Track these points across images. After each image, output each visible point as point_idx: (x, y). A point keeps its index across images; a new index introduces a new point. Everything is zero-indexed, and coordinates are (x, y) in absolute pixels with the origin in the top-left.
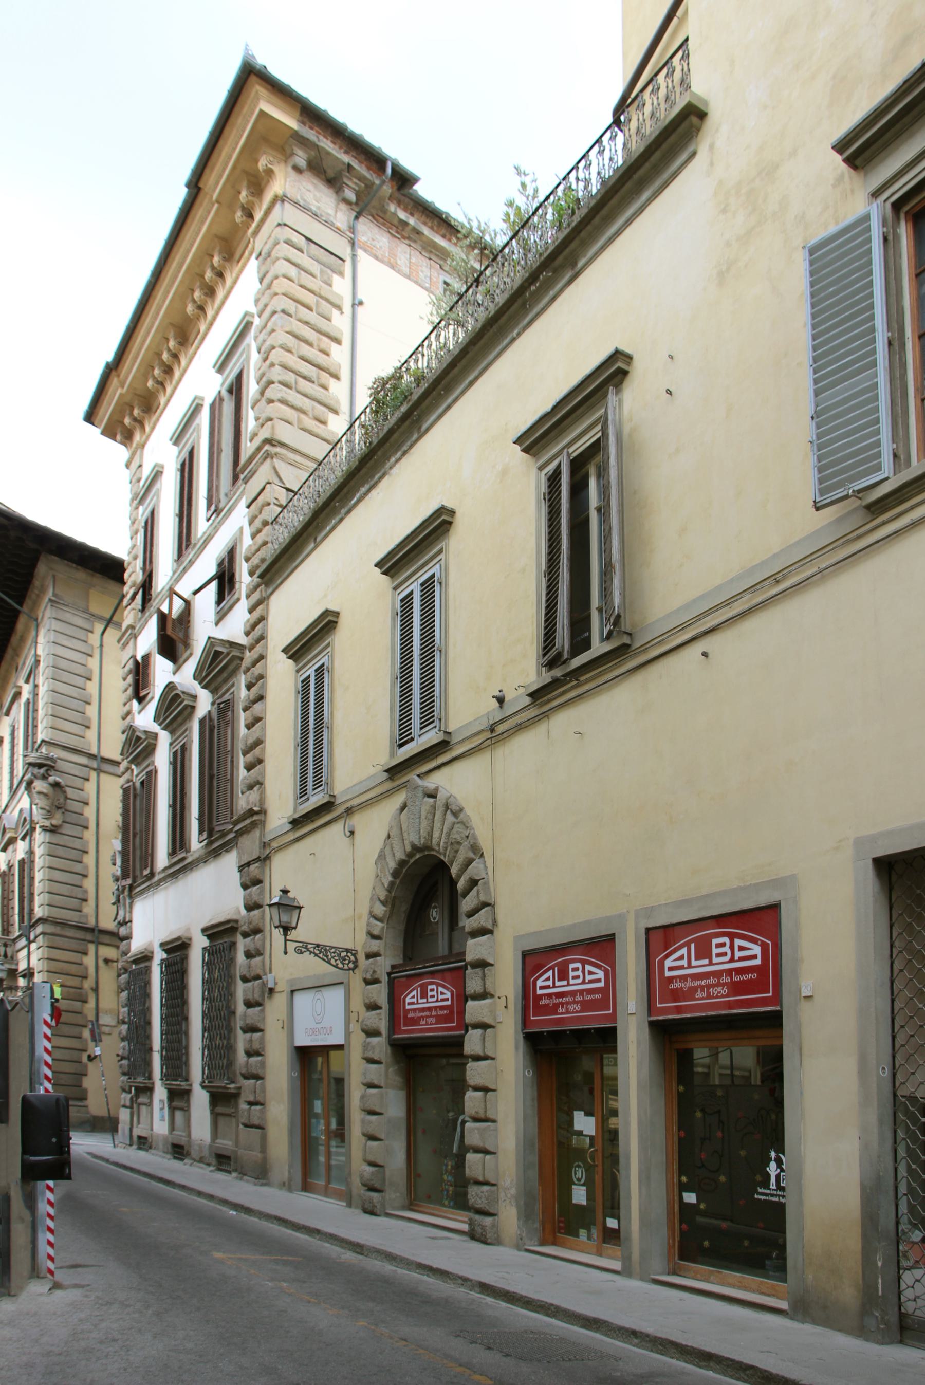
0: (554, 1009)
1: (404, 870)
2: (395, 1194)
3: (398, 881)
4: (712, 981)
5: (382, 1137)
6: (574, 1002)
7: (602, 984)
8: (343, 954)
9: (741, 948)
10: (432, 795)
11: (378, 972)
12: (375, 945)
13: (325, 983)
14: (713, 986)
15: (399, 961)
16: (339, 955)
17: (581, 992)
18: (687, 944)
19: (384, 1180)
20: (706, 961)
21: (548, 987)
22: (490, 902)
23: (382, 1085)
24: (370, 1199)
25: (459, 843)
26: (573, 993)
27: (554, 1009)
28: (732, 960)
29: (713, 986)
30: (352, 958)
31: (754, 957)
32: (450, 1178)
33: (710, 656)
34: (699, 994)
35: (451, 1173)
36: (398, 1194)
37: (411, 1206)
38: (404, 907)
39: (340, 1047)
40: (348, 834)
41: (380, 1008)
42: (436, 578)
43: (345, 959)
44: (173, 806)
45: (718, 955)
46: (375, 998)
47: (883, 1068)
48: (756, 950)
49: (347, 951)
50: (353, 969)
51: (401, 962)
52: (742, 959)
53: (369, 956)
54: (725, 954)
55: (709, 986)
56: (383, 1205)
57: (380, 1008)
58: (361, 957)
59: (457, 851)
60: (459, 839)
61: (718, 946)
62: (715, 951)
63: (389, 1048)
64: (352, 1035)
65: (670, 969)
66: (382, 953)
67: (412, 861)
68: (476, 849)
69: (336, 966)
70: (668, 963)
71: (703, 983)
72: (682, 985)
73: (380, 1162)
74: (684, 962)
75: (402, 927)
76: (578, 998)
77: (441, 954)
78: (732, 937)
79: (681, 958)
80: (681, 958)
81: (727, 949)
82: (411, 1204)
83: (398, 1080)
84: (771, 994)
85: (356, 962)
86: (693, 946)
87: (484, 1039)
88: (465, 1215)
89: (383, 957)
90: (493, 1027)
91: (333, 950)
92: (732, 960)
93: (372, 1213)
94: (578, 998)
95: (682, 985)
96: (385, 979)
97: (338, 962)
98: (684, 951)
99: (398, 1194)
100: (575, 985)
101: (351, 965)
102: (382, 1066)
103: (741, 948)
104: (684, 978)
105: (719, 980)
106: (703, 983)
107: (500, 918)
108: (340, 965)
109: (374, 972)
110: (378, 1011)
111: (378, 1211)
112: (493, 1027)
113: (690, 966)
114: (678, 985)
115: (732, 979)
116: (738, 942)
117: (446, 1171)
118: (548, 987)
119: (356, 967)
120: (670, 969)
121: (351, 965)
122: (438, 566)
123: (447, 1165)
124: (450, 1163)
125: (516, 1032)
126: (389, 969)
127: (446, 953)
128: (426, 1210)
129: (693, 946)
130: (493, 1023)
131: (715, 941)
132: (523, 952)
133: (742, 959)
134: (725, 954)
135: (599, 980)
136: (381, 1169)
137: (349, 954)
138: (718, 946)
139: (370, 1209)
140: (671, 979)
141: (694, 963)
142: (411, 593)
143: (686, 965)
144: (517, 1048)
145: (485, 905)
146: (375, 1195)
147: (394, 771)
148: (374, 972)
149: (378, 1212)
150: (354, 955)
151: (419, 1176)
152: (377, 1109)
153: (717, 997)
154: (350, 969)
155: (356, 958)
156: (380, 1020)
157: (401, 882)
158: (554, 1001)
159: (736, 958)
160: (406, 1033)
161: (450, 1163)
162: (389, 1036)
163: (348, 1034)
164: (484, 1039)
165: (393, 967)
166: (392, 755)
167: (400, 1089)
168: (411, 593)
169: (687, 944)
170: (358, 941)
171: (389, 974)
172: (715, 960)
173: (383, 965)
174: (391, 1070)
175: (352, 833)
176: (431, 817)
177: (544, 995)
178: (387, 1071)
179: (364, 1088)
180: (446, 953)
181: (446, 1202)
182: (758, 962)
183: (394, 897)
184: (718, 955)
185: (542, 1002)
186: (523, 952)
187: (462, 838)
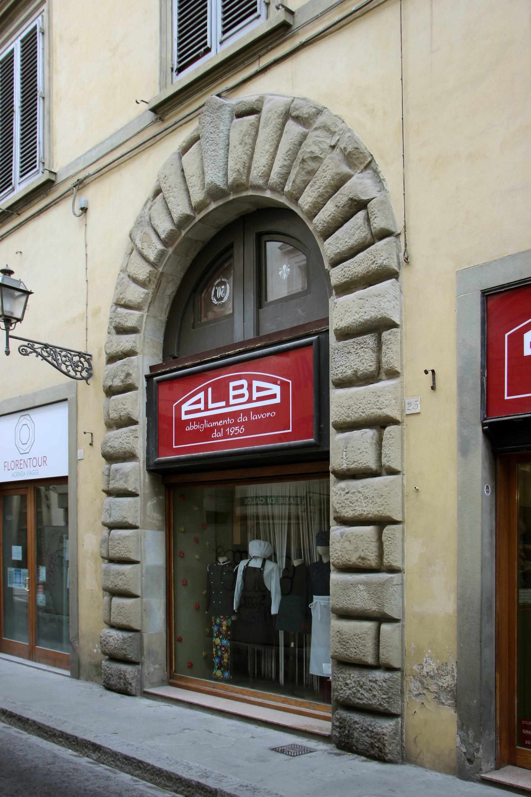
0: (207, 434)
1: (183, 233)
2: (154, 667)
3: (170, 250)
4: (229, 421)
5: (139, 593)
6: (236, 424)
7: (277, 400)
8: (76, 359)
9: (259, 389)
10: (253, 111)
11: (134, 375)
12: (126, 342)
13: (37, 404)
14: (230, 426)
15: (158, 361)
16: (71, 360)
17: (246, 412)
18: (205, 389)
19: (141, 648)
20: (223, 404)
21: (199, 411)
22: (393, 230)
23: (138, 524)
24: (117, 672)
25: (315, 158)
26: (235, 415)
27: (207, 434)
28: (250, 400)
29: (230, 426)
30: (86, 365)
31: (274, 396)
32: (225, 642)
33: (23, 253)
34: (215, 435)
35: (226, 637)
36: (157, 666)
37: (172, 679)
38: (170, 290)
39: (63, 480)
40: (78, 212)
41: (135, 423)
42: (38, 30)
43: (75, 364)
44: (6, 42)
45: (235, 397)
46: (129, 409)
47: (487, 487)
48: (276, 389)
49: (80, 355)
50: (86, 379)
51: (160, 362)
52: (259, 399)
53: (112, 359)
54: (242, 396)
55: (225, 426)
56: (141, 683)
57: (135, 423)
58: (99, 363)
59: (311, 173)
60: (317, 152)
61: (235, 388)
62: (232, 393)
63: (147, 475)
64: (81, 464)
65: (187, 413)
66: (138, 350)
67: (199, 217)
68: (358, 159)
69: (67, 374)
70: (185, 407)
71: (220, 423)
72: (198, 427)
73: (135, 625)
74: (201, 406)
75: (164, 317)
76: (241, 419)
77: (238, 337)
78: (250, 379)
79: (198, 402)
80: (198, 402)
81: (245, 391)
82: (171, 676)
83: (155, 517)
84: (174, 447)
85: (90, 369)
86: (210, 390)
87: (379, 443)
88: (324, 709)
89: (139, 356)
90: (395, 422)
91: (64, 353)
92: (250, 400)
93: (125, 692)
94: (241, 419)
95: (198, 427)
96: (142, 384)
97: (70, 368)
98: (201, 395)
99: (157, 666)
100: (237, 405)
101: (84, 374)
102: (137, 499)
103: (259, 389)
104: (200, 420)
105: (236, 420)
106: (220, 423)
107: (415, 251)
108: (72, 373)
109: (128, 375)
110: (133, 427)
111: (134, 687)
112: (395, 422)
113: (206, 409)
114: (194, 427)
115: (249, 418)
116: (256, 384)
117: (219, 633)
118: (199, 411)
119: (90, 375)
120: (187, 413)
121: (84, 374)
122: (40, 18)
123: (220, 625)
124: (225, 623)
125: (463, 423)
126: (147, 372)
127: (251, 335)
128: (190, 685)
129: (210, 390)
130: (399, 418)
131: (232, 384)
132: (483, 292)
133: (259, 399)
134: (242, 396)
135: (274, 396)
136: (137, 635)
137: (82, 360)
138: (235, 388)
139: (122, 686)
140: (187, 422)
141: (211, 406)
142: (12, 51)
143: (203, 409)
144: (464, 450)
145: (384, 234)
146: (128, 669)
147: (161, 110)
148: (128, 375)
149: (134, 692)
150: (88, 361)
151: (180, 640)
152: (133, 557)
153: (234, 436)
154: (83, 378)
155: (90, 365)
156: (136, 439)
157: (174, 252)
158: (206, 425)
159: (254, 398)
160: (176, 453)
161: (225, 623)
162: (148, 459)
163: (74, 461)
164: (379, 443)
165: (152, 368)
166: (163, 86)
167: (159, 529)
168: (12, 51)
169: (205, 389)
170: (97, 341)
171: (148, 378)
172: (232, 401)
173: (140, 367)
174: (149, 504)
175: (84, 210)
176: (249, 141)
177: (192, 420)
178: (145, 505)
179: (106, 530)
180: (251, 335)
181: (219, 673)
182: (277, 400)
183: (162, 273)
184: (235, 397)
185: (188, 429)
186: (483, 292)
187: (323, 150)
